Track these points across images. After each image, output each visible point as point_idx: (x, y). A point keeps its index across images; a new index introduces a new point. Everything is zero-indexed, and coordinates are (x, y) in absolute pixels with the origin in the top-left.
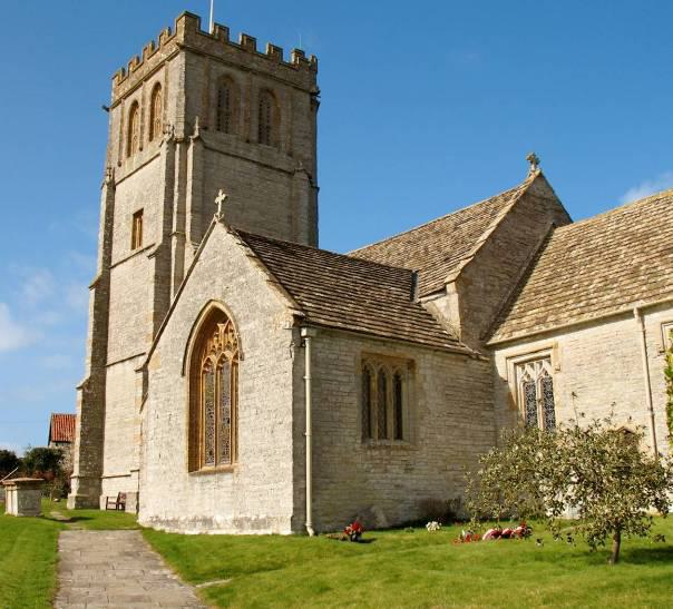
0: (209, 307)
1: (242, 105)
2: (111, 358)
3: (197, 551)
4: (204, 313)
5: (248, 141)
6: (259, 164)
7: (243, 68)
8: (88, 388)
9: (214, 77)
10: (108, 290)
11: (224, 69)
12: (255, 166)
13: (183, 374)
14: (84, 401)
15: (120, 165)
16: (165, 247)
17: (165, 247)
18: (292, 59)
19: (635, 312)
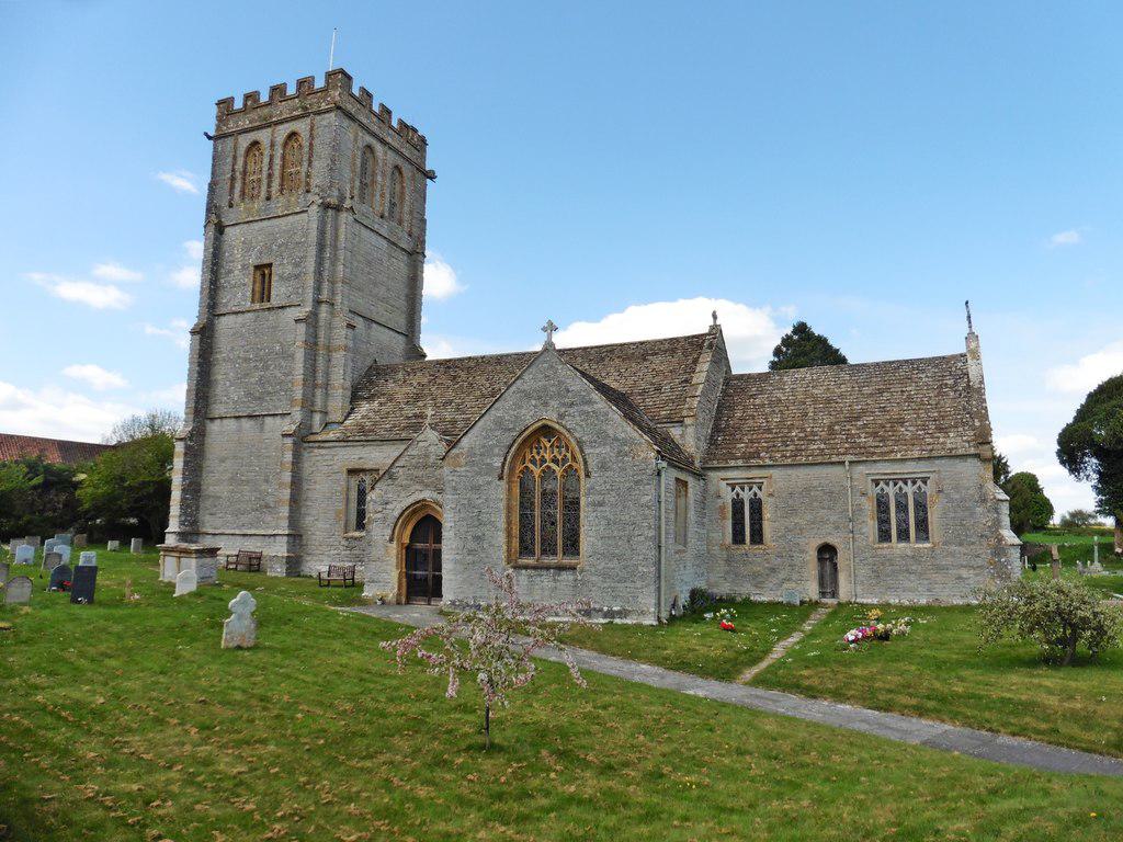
0: (540, 424)
1: (379, 178)
2: (218, 409)
3: (991, 665)
4: (531, 429)
5: (382, 217)
6: (389, 241)
7: (383, 142)
8: (191, 439)
9: (360, 144)
10: (211, 337)
11: (369, 139)
12: (384, 243)
13: (501, 478)
14: (186, 454)
15: (231, 206)
16: (314, 314)
17: (314, 314)
18: (395, 123)
19: (847, 463)
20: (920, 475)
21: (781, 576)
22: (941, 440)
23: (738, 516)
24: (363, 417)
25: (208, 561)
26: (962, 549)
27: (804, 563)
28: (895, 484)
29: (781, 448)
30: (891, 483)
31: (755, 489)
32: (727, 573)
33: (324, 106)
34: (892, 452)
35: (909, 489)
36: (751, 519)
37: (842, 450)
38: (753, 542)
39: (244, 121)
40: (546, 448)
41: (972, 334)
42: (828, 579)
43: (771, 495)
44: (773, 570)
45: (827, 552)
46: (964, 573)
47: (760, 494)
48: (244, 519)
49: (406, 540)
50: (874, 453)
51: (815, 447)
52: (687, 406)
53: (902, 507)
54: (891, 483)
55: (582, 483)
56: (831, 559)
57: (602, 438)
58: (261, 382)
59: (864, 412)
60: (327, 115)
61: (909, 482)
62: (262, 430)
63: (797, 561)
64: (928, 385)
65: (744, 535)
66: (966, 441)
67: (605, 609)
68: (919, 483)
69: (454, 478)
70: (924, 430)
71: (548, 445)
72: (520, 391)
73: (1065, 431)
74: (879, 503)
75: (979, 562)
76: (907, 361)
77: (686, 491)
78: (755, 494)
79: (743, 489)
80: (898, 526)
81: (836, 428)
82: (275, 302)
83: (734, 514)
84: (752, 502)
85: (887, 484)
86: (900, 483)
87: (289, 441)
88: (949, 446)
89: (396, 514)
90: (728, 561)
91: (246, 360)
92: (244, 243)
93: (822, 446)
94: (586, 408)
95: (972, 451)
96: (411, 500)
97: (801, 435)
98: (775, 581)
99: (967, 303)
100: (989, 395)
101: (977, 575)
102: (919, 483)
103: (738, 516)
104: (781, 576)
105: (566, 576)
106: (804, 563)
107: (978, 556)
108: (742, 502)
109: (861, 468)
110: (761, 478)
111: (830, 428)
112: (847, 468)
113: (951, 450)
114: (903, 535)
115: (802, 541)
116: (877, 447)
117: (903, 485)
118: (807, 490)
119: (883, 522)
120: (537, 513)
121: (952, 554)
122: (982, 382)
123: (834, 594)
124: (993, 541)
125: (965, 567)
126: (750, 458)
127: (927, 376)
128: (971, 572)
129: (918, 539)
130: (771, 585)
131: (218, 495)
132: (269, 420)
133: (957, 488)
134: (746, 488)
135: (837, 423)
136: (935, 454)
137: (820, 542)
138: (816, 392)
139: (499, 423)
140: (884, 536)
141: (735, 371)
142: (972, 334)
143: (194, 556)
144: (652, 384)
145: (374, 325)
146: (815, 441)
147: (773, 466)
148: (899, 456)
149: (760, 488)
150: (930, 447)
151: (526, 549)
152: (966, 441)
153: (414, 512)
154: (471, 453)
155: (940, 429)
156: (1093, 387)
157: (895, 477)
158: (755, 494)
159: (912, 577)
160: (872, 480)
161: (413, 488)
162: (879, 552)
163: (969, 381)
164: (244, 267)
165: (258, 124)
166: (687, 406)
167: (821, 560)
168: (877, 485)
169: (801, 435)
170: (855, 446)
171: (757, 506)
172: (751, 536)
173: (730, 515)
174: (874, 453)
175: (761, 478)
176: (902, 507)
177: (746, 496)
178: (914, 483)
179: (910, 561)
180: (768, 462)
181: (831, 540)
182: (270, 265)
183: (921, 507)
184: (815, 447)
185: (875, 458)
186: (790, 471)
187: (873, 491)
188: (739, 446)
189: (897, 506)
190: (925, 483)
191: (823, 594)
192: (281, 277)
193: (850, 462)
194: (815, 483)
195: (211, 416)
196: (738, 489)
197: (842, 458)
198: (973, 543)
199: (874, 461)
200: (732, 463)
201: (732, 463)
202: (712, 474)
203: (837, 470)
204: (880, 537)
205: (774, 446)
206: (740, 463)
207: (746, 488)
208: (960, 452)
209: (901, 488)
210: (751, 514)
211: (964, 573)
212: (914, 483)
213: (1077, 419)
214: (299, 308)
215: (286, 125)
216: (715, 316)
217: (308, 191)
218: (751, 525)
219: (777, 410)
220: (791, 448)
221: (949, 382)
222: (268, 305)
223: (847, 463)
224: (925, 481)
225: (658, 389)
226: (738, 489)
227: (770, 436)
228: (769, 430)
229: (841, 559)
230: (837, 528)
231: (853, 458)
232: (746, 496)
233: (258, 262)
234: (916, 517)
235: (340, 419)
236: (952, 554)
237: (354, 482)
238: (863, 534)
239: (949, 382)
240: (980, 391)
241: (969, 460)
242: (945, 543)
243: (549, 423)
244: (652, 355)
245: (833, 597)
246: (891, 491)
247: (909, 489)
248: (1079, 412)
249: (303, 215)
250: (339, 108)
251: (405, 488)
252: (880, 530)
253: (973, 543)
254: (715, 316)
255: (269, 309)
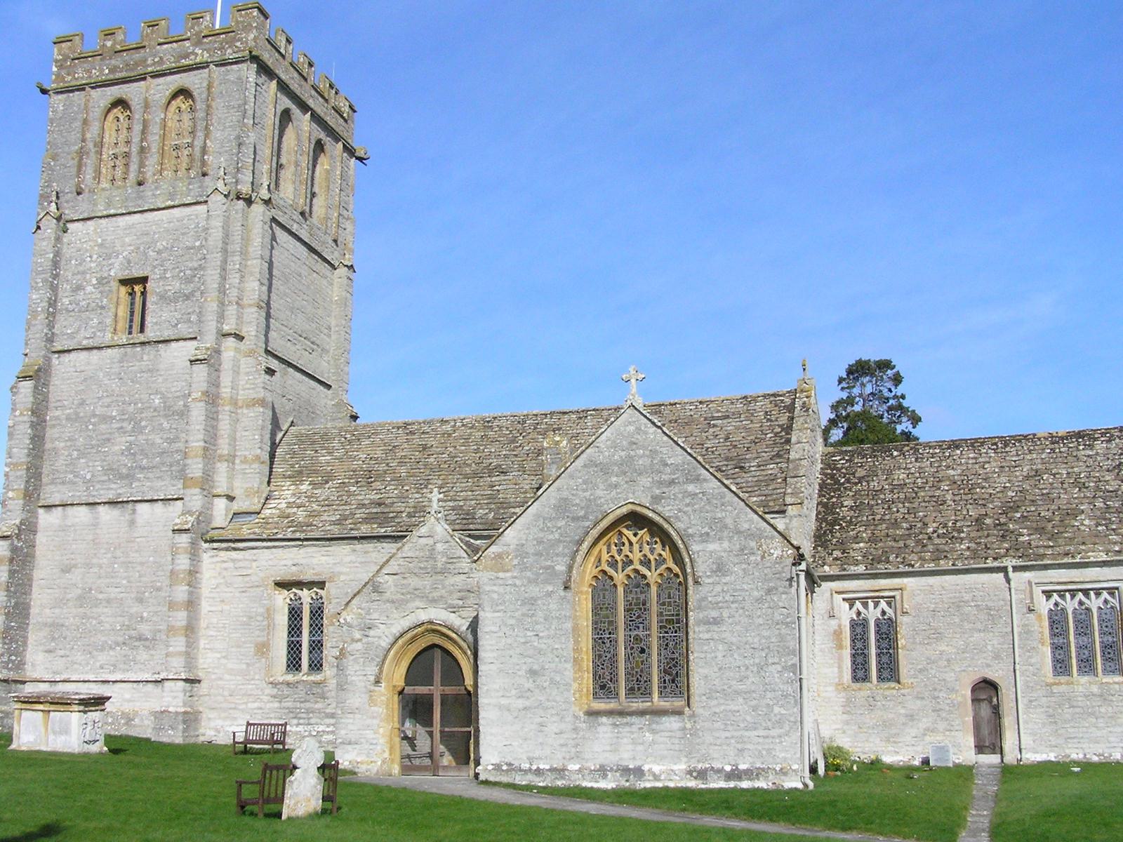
8: (19, 539)
9: (280, 109)
24: (290, 505)
25: (95, 715)
28: (1073, 597)
33: (230, 54)
39: (101, 70)
40: (631, 544)
45: (986, 689)
47: (890, 611)
48: (103, 658)
49: (400, 682)
50: (1043, 556)
53: (1083, 626)
55: (690, 592)
57: (718, 528)
58: (129, 451)
60: (235, 67)
62: (132, 523)
67: (728, 768)
69: (495, 588)
71: (634, 540)
72: (592, 463)
82: (150, 334)
85: (1063, 597)
86: (1080, 596)
87: (184, 539)
89: (385, 643)
91: (106, 419)
92: (101, 245)
94: (691, 488)
96: (406, 623)
98: (914, 732)
102: (1105, 595)
105: (671, 723)
114: (1087, 665)
119: (1060, 650)
120: (621, 635)
123: (997, 748)
131: (61, 621)
132: (140, 506)
134: (871, 604)
137: (977, 677)
139: (562, 507)
140: (1061, 666)
143: (76, 708)
145: (291, 370)
146: (962, 539)
151: (603, 687)
153: (413, 640)
154: (521, 551)
157: (1074, 587)
159: (1101, 722)
161: (412, 605)
164: (102, 281)
165: (124, 74)
168: (851, 606)
171: (294, 663)
173: (847, 642)
174: (1043, 556)
177: (872, 614)
178: (1098, 594)
181: (991, 675)
182: (144, 280)
187: (1044, 606)
192: (163, 297)
195: (215, 492)
207: (871, 604)
212: (1098, 594)
214: (194, 343)
215: (170, 78)
217: (204, 175)
222: (142, 338)
226: (858, 605)
233: (126, 274)
235: (257, 508)
237: (282, 599)
243: (639, 509)
249: (198, 207)
250: (254, 59)
251: (397, 604)
255: (143, 343)
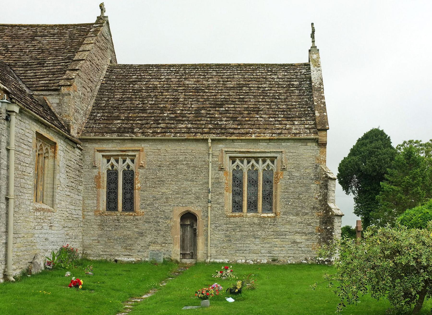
19: (210, 141)
20: (269, 155)
21: (148, 239)
22: (288, 126)
23: (128, 196)
26: (299, 219)
27: (169, 228)
28: (249, 162)
29: (154, 126)
30: (245, 161)
31: (128, 161)
32: (100, 236)
34: (247, 133)
35: (260, 167)
36: (124, 189)
37: (206, 130)
38: (125, 209)
41: (314, 47)
42: (188, 243)
43: (141, 167)
44: (141, 234)
46: (298, 238)
50: (233, 134)
51: (183, 126)
52: (65, 77)
53: (253, 183)
54: (245, 161)
56: (192, 226)
59: (226, 101)
61: (260, 160)
63: (162, 227)
64: (279, 84)
65: (116, 203)
66: (307, 128)
68: (268, 162)
70: (275, 118)
73: (343, 162)
74: (235, 179)
75: (310, 229)
76: (263, 65)
77: (55, 153)
78: (128, 166)
79: (117, 161)
80: (249, 198)
81: (203, 111)
83: (109, 183)
84: (125, 173)
86: (253, 161)
88: (294, 131)
90: (101, 226)
93: (189, 126)
95: (312, 136)
97: (172, 116)
99: (312, 24)
100: (327, 94)
101: (308, 240)
102: (268, 162)
103: (113, 186)
104: (148, 239)
106: (169, 228)
107: (309, 225)
108: (116, 173)
109: (221, 146)
110: (133, 151)
111: (198, 110)
112: (210, 144)
113: (295, 134)
114: (253, 206)
115: (167, 209)
116: (235, 129)
117: (255, 163)
118: (175, 163)
121: (289, 223)
122: (321, 84)
123: (193, 255)
124: (322, 213)
125: (299, 233)
126: (124, 132)
127: (278, 78)
128: (304, 237)
129: (264, 210)
130: (139, 247)
133: (298, 167)
134: (121, 160)
135: (203, 108)
136: (282, 137)
137: (183, 210)
138: (187, 82)
141: (121, 60)
142: (314, 47)
144: (36, 59)
147: (144, 140)
148: (253, 137)
149: (133, 161)
150: (279, 131)
152: (307, 128)
155: (287, 118)
156: (361, 135)
158: (128, 166)
159: (257, 241)
160: (230, 157)
162: (232, 220)
163: (311, 84)
166: (65, 77)
167: (183, 226)
168: (233, 162)
169: (172, 116)
170: (217, 127)
172: (124, 203)
174: (233, 134)
175: (133, 151)
176: (253, 183)
177: (120, 167)
178: (264, 161)
179: (256, 228)
180: (140, 136)
181: (193, 209)
183: (268, 182)
184: (183, 126)
185: (233, 137)
186: (160, 146)
188: (115, 122)
189: (249, 181)
190: (273, 162)
191: (184, 255)
193: (212, 140)
194: (181, 158)
196: (112, 160)
197: (206, 136)
198: (307, 214)
199: (233, 140)
200: (108, 136)
201: (108, 136)
202: (89, 146)
203: (201, 147)
204: (233, 207)
205: (147, 124)
206: (115, 136)
207: (121, 160)
208: (303, 136)
209: (253, 166)
210: (124, 184)
211: (298, 238)
212: (264, 161)
213: (350, 155)
216: (102, 7)
218: (124, 194)
219: (152, 94)
220: (162, 125)
221: (295, 83)
223: (210, 141)
224: (273, 159)
225: (41, 64)
226: (112, 160)
227: (145, 115)
228: (144, 110)
229: (200, 226)
230: (197, 198)
231: (214, 136)
232: (120, 167)
234: (264, 191)
236: (289, 223)
238: (218, 204)
239: (295, 83)
240: (320, 90)
241: (309, 144)
242: (285, 213)
244: (41, 36)
245: (192, 258)
246: (245, 167)
247: (260, 167)
248: (352, 150)
252: (234, 202)
253: (307, 214)
254: (102, 7)
